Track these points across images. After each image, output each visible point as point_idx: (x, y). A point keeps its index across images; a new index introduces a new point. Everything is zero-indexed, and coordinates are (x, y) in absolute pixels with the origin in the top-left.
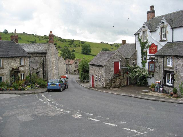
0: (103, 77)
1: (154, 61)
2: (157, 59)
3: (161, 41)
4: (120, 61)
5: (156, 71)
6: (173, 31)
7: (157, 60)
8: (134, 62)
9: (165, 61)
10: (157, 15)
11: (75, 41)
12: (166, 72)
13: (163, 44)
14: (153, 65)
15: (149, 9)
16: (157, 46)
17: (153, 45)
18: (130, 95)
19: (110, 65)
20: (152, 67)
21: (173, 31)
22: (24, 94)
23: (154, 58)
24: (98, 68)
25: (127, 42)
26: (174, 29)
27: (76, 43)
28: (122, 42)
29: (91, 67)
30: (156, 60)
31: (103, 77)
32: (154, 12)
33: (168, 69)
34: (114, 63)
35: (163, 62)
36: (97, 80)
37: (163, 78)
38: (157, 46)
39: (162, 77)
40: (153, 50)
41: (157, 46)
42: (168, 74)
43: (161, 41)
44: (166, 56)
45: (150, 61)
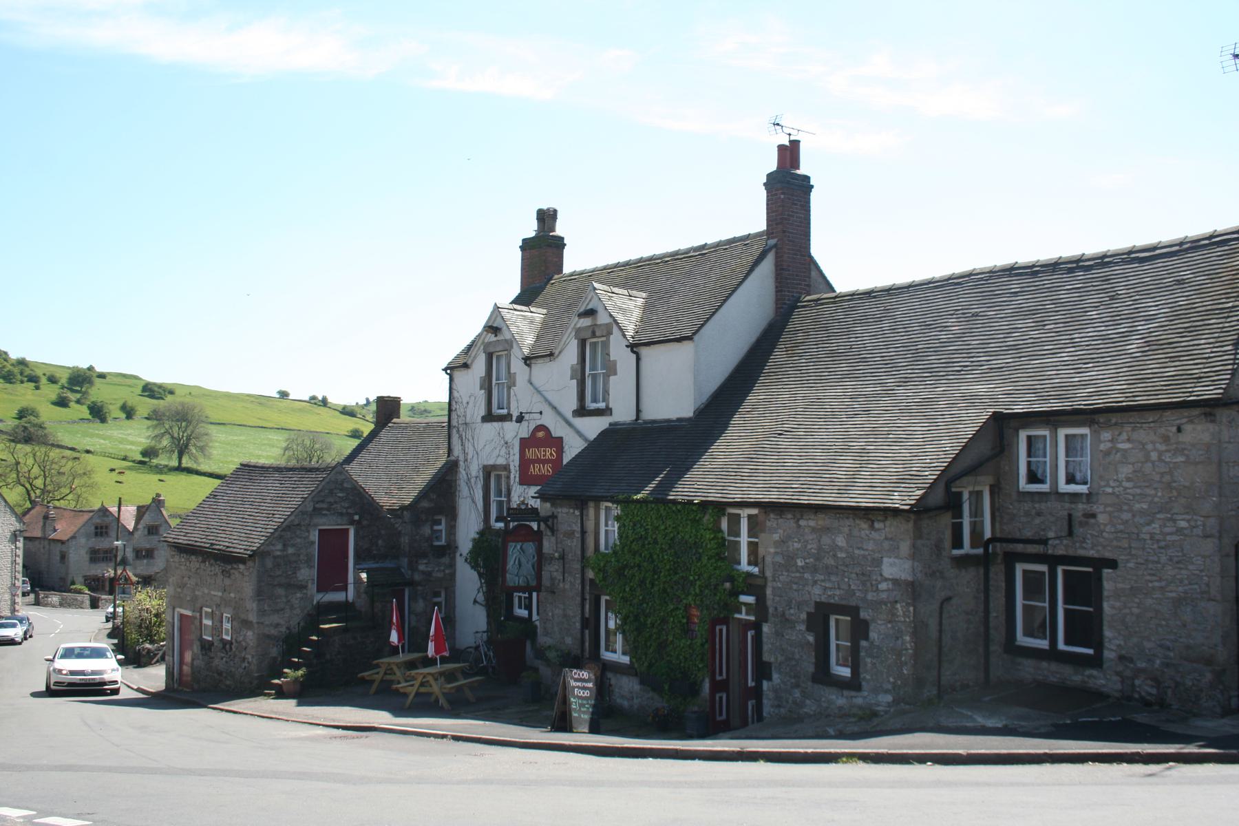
0: (246, 624)
1: (535, 526)
2: (554, 517)
3: (582, 411)
4: (352, 522)
5: (546, 582)
6: (638, 359)
7: (550, 521)
10: (572, 263)
11: (102, 376)
13: (593, 427)
14: (530, 547)
15: (530, 229)
17: (541, 434)
19: (290, 550)
20: (523, 560)
21: (638, 359)
22: (977, 784)
23: (534, 511)
26: (644, 351)
27: (98, 393)
28: (778, 150)
30: (545, 520)
31: (617, 508)
32: (559, 244)
34: (314, 536)
35: (583, 532)
37: (585, 623)
39: (578, 618)
43: (582, 411)
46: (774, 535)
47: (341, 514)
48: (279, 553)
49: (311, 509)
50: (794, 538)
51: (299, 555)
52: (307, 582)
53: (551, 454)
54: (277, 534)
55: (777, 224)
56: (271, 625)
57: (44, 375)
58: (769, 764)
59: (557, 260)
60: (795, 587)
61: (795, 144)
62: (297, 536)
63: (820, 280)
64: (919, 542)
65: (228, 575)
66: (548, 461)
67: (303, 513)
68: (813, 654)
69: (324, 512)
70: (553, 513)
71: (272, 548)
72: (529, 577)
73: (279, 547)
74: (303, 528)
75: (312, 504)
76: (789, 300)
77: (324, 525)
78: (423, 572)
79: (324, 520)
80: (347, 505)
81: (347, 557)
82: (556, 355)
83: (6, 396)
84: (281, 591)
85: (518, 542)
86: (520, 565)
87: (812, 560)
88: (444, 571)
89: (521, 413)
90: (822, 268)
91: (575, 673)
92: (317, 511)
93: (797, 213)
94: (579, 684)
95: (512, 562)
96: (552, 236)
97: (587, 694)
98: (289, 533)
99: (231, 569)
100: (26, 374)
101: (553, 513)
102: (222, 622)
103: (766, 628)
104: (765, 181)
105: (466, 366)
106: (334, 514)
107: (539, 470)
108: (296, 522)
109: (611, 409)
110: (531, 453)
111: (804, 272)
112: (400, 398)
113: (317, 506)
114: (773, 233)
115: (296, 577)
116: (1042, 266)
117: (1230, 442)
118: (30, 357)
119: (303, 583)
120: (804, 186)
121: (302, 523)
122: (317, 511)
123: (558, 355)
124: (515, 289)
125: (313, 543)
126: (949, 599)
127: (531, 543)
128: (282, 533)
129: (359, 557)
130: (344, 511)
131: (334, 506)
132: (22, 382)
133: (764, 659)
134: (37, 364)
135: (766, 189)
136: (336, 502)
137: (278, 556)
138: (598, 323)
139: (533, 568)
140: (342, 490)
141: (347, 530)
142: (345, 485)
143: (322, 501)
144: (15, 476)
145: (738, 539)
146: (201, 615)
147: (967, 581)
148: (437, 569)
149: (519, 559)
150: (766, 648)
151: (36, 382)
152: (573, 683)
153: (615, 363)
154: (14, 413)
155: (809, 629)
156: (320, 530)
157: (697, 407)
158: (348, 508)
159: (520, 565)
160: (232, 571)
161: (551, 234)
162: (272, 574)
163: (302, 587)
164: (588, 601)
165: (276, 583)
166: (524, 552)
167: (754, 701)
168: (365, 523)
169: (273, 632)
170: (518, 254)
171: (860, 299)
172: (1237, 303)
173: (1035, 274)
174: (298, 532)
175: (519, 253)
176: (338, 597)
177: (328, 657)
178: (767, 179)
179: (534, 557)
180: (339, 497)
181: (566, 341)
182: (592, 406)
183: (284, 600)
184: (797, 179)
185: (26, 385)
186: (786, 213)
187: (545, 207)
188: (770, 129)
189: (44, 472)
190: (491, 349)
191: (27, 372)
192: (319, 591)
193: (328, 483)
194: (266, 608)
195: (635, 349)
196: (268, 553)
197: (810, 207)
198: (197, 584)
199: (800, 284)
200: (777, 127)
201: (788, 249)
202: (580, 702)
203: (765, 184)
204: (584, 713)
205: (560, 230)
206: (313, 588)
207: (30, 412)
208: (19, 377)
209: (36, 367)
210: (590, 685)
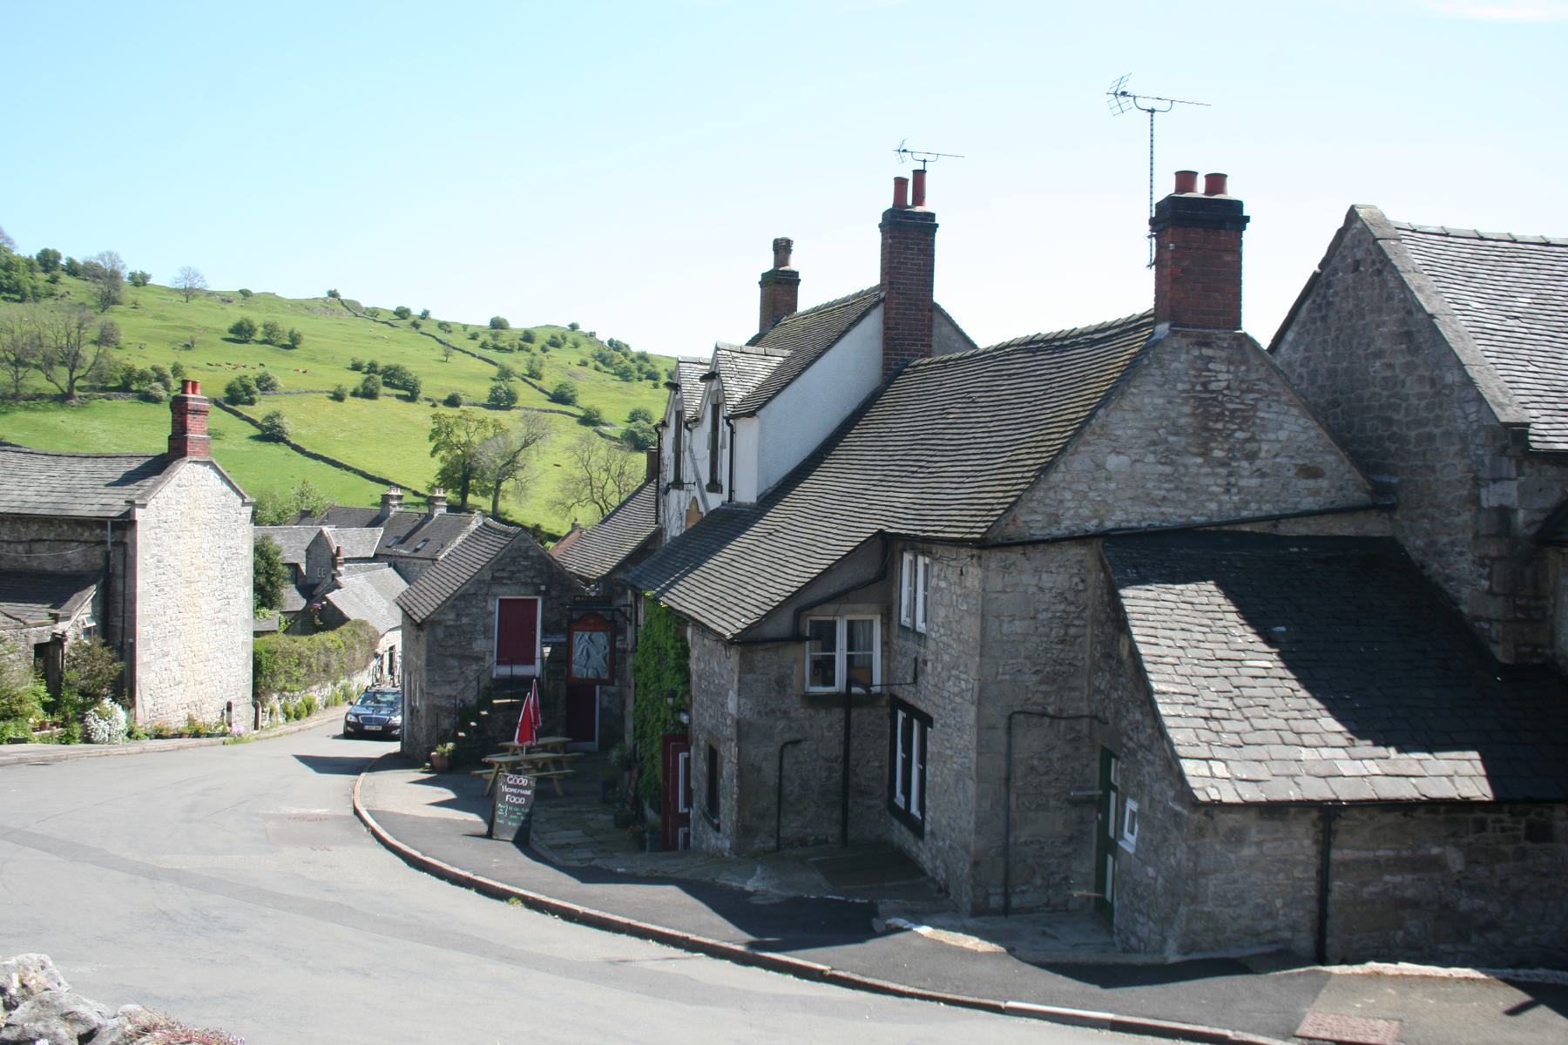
4: (538, 593)
10: (807, 299)
19: (465, 620)
20: (592, 651)
34: (494, 606)
47: (526, 584)
48: (452, 623)
49: (489, 578)
51: (475, 626)
52: (485, 655)
54: (448, 603)
56: (442, 696)
57: (666, 370)
58: (481, 896)
59: (788, 298)
62: (474, 606)
63: (955, 337)
64: (749, 677)
67: (480, 582)
69: (505, 581)
71: (443, 617)
72: (599, 669)
73: (452, 616)
74: (480, 597)
75: (490, 572)
76: (895, 364)
77: (505, 594)
79: (504, 589)
80: (532, 574)
81: (535, 630)
83: (621, 396)
84: (453, 662)
85: (586, 631)
86: (588, 655)
90: (957, 322)
91: (511, 779)
92: (496, 580)
93: (913, 259)
94: (514, 790)
96: (783, 271)
97: (521, 801)
98: (463, 603)
100: (644, 370)
104: (880, 221)
106: (517, 584)
108: (472, 591)
111: (921, 330)
113: (497, 574)
115: (471, 648)
116: (1019, 345)
117: (1004, 592)
118: (651, 351)
119: (480, 655)
120: (927, 225)
121: (479, 592)
122: (496, 580)
124: (755, 330)
125: (492, 613)
126: (796, 742)
128: (456, 602)
129: (546, 630)
130: (529, 580)
131: (518, 575)
132: (640, 379)
134: (660, 359)
136: (519, 571)
137: (450, 626)
140: (527, 558)
141: (536, 601)
142: (531, 553)
143: (503, 570)
144: (589, 491)
147: (828, 725)
149: (587, 650)
151: (654, 379)
152: (505, 789)
154: (626, 416)
156: (501, 600)
157: (762, 491)
158: (533, 577)
159: (588, 655)
161: (781, 269)
162: (443, 643)
163: (479, 659)
165: (448, 653)
168: (554, 593)
170: (757, 292)
171: (938, 368)
173: (1063, 348)
174: (474, 602)
175: (758, 290)
176: (521, 670)
177: (490, 733)
183: (457, 671)
184: (913, 219)
185: (644, 383)
186: (896, 261)
189: (619, 487)
191: (647, 367)
193: (510, 550)
194: (437, 678)
196: (440, 623)
197: (933, 250)
199: (913, 345)
200: (1122, 99)
201: (897, 304)
202: (511, 808)
204: (513, 820)
205: (794, 264)
207: (643, 415)
208: (637, 374)
209: (659, 361)
210: (528, 792)
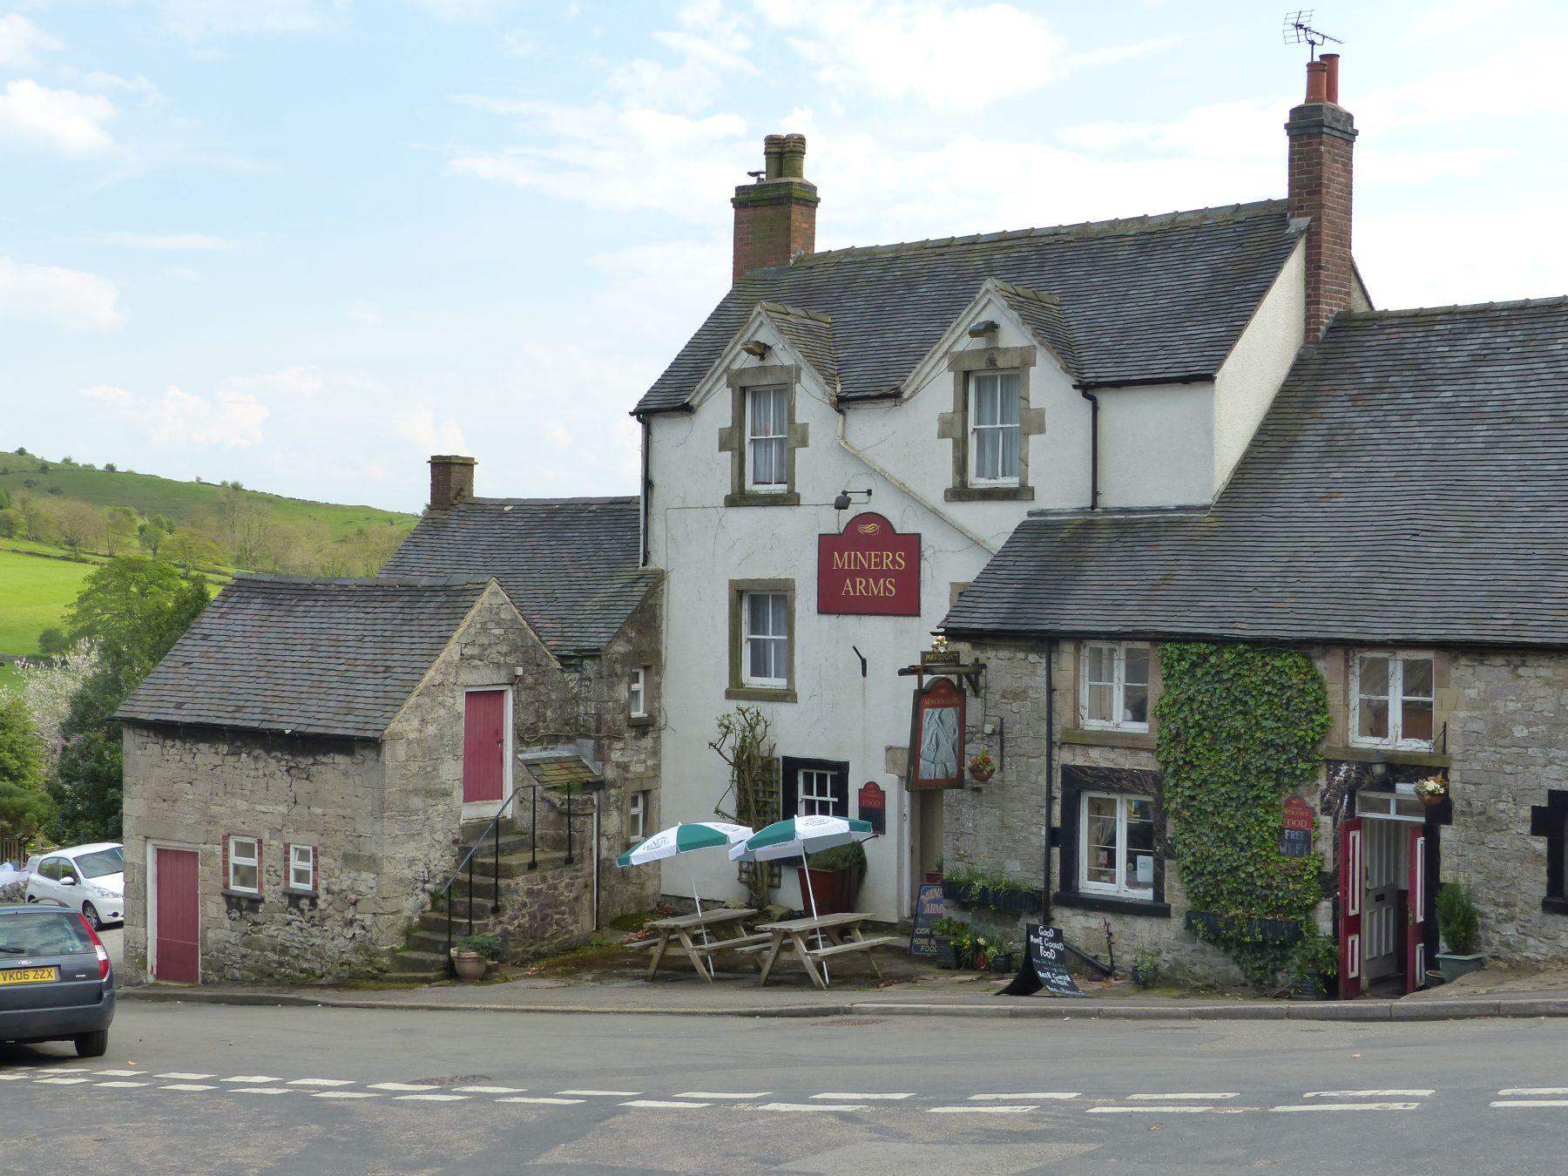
2: (979, 667)
6: (1095, 409)
8: (636, 693)
9: (1063, 678)
12: (1075, 781)
14: (950, 714)
15: (749, 163)
16: (916, 538)
17: (869, 528)
18: (885, 999)
19: (431, 730)
21: (1095, 409)
24: (274, 765)
25: (485, 486)
26: (1105, 398)
29: (130, 740)
32: (809, 200)
33: (1098, 758)
34: (461, 704)
36: (254, 903)
37: (1053, 837)
38: (916, 538)
40: (865, 573)
41: (912, 544)
42: (1091, 800)
43: (961, 493)
44: (1078, 638)
45: (927, 678)
46: (1468, 691)
47: (498, 665)
50: (1506, 695)
53: (894, 562)
55: (1308, 193)
60: (1508, 769)
61: (1330, 60)
65: (305, 776)
66: (886, 574)
68: (1545, 869)
70: (977, 660)
73: (416, 723)
75: (458, 648)
78: (618, 765)
82: (905, 396)
84: (416, 802)
87: (1543, 727)
88: (645, 761)
89: (845, 493)
95: (928, 741)
99: (313, 764)
101: (977, 660)
102: (287, 859)
103: (1446, 833)
104: (1287, 121)
105: (687, 409)
107: (866, 588)
109: (1032, 490)
110: (841, 561)
112: (473, 459)
114: (1301, 208)
120: (1345, 132)
123: (908, 399)
127: (951, 709)
133: (1442, 880)
135: (1288, 134)
138: (1002, 345)
139: (954, 749)
145: (1363, 696)
146: (226, 850)
148: (635, 758)
150: (1445, 863)
153: (1041, 414)
155: (1536, 831)
158: (506, 655)
160: (314, 769)
163: (446, 794)
164: (1059, 801)
165: (410, 787)
166: (942, 723)
167: (1422, 945)
169: (408, 873)
172: (1566, 329)
178: (1291, 118)
179: (955, 730)
180: (495, 636)
181: (928, 374)
182: (977, 482)
187: (784, 133)
188: (1286, 34)
190: (747, 381)
192: (468, 798)
195: (1089, 392)
198: (213, 794)
203: (1287, 126)
206: (459, 793)
